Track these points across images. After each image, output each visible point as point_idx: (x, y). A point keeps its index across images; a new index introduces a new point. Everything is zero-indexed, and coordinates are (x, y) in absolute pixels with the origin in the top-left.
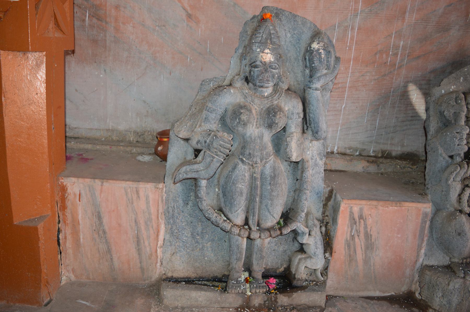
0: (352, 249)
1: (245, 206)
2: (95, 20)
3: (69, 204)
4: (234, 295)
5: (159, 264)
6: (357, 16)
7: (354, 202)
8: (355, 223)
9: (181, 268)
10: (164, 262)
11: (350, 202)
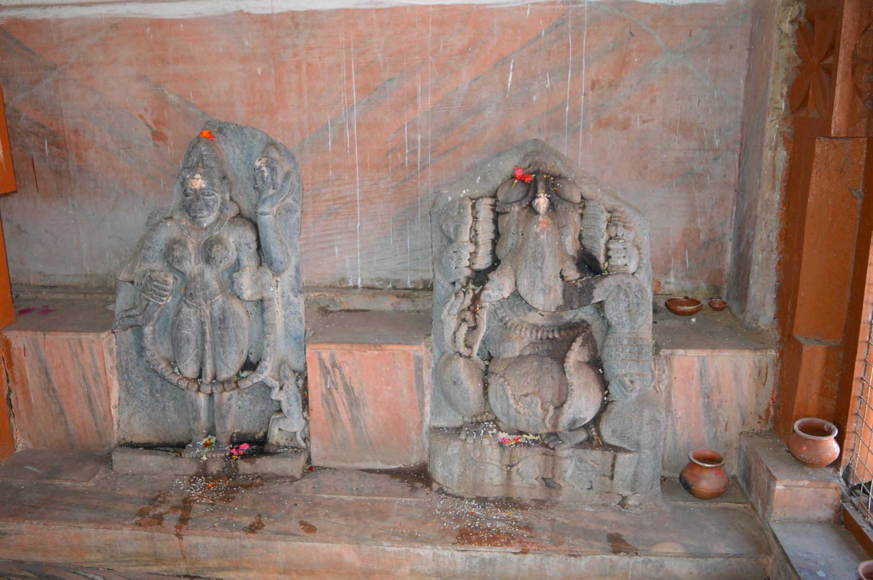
0: (333, 407)
1: (197, 355)
2: (54, 149)
3: (15, 360)
4: (188, 461)
5: (115, 427)
6: (353, 109)
7: (321, 346)
8: (329, 373)
9: (141, 432)
10: (122, 425)
11: (315, 346)
